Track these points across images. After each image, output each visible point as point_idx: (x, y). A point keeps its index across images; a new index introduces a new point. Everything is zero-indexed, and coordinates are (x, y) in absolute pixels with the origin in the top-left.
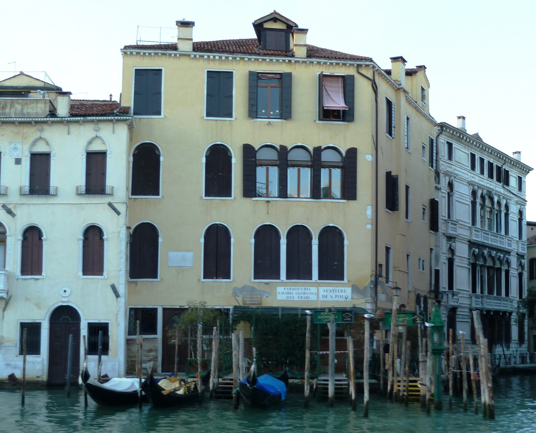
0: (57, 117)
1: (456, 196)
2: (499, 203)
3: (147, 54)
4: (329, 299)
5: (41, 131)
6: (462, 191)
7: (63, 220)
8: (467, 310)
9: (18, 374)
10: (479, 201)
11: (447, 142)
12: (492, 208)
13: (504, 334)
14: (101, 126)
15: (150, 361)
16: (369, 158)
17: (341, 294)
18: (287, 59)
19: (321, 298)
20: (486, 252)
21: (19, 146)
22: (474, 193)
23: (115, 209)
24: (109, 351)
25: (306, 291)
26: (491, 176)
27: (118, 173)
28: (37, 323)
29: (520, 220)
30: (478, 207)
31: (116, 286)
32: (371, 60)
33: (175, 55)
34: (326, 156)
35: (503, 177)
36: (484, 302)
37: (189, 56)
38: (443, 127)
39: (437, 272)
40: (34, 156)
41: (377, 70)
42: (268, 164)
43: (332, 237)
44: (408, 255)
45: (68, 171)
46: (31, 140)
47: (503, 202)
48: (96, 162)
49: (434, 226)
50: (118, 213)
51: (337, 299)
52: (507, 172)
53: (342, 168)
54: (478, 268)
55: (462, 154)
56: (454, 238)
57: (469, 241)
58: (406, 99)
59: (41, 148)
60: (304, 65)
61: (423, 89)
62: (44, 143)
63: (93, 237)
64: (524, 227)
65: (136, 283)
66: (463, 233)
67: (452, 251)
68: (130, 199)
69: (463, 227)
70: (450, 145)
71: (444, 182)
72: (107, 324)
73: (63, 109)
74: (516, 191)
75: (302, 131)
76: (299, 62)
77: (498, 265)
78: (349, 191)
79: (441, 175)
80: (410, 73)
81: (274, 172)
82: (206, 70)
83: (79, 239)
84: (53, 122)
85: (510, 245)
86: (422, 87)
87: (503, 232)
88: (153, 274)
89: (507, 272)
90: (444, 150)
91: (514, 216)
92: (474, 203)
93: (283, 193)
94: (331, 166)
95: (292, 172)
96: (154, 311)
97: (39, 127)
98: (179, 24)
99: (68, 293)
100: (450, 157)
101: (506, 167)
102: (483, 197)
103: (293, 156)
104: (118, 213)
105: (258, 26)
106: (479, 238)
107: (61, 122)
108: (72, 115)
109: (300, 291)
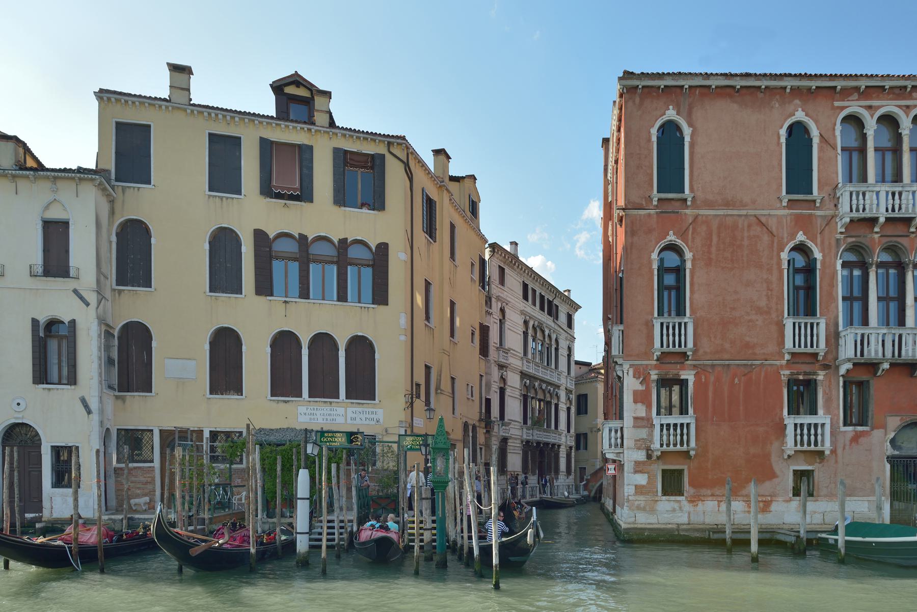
1: (508, 324)
2: (549, 336)
4: (358, 420)
6: (515, 320)
8: (519, 441)
10: (530, 331)
13: (553, 466)
14: (60, 184)
15: (145, 495)
17: (372, 416)
18: (306, 127)
19: (349, 421)
20: (537, 384)
22: (526, 323)
23: (81, 298)
29: (569, 356)
30: (530, 339)
31: (87, 399)
32: (403, 138)
34: (354, 253)
35: (552, 311)
37: (185, 110)
38: (494, 247)
39: (488, 401)
41: (412, 153)
43: (361, 348)
44: (453, 379)
47: (554, 337)
49: (484, 350)
50: (87, 304)
51: (367, 422)
52: (557, 307)
53: (373, 266)
54: (529, 400)
55: (514, 281)
56: (507, 367)
65: (123, 399)
66: (515, 362)
67: (503, 380)
68: (115, 290)
70: (502, 270)
75: (323, 218)
76: (320, 131)
78: (380, 296)
79: (493, 300)
81: (294, 267)
82: (207, 132)
85: (559, 379)
87: (553, 366)
88: (147, 387)
89: (557, 406)
91: (563, 352)
92: (525, 334)
95: (314, 269)
100: (502, 281)
101: (556, 302)
103: (315, 250)
104: (87, 304)
105: (278, 88)
106: (531, 370)
109: (326, 412)
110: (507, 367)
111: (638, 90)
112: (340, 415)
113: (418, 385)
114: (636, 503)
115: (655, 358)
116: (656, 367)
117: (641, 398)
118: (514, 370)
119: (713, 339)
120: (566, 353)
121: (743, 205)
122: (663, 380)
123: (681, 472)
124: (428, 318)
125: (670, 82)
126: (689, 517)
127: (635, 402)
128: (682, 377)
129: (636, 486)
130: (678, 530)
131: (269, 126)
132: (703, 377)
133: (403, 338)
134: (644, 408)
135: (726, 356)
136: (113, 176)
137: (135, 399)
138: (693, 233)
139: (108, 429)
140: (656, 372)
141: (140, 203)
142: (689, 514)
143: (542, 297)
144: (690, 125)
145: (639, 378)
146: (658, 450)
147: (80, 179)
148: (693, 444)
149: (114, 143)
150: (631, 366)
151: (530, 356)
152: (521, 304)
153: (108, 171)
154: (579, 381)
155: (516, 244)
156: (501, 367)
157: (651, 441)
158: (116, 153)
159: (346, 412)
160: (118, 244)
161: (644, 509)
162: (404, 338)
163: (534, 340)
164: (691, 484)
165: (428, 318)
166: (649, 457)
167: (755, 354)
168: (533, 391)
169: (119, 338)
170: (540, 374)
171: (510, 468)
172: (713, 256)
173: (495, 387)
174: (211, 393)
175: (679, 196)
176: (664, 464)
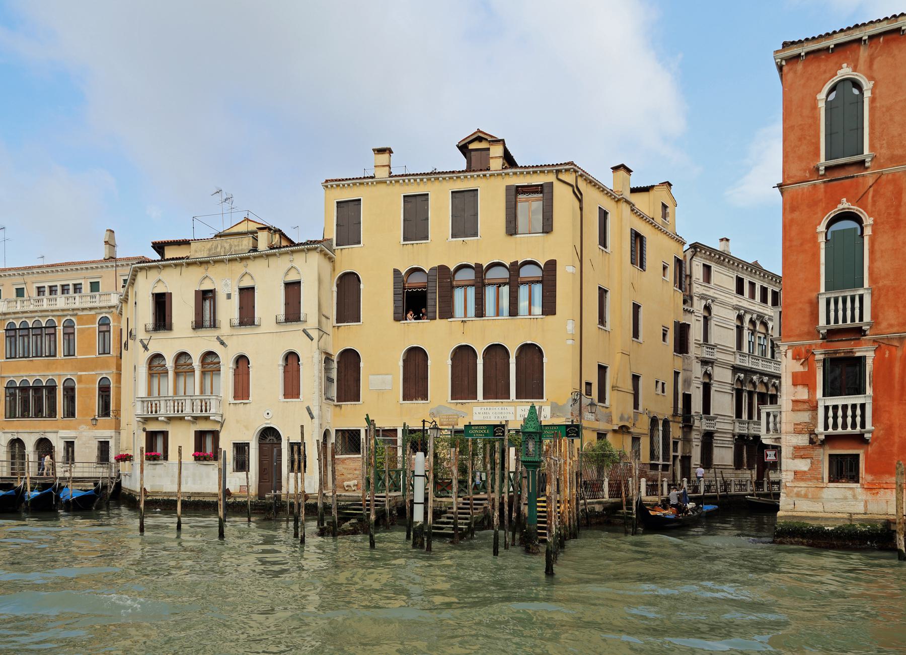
5: (246, 266)
6: (725, 316)
7: (266, 345)
11: (704, 265)
14: (296, 256)
20: (755, 378)
21: (229, 282)
22: (740, 318)
23: (308, 335)
30: (746, 333)
32: (572, 163)
33: (372, 183)
36: (750, 428)
39: (687, 398)
40: (242, 290)
41: (581, 176)
43: (531, 354)
45: (270, 304)
46: (239, 275)
48: (293, 288)
50: (312, 339)
55: (724, 278)
56: (712, 363)
58: (632, 210)
59: (246, 283)
60: (500, 177)
61: (665, 207)
67: (708, 375)
69: (724, 351)
70: (707, 269)
71: (698, 306)
73: (263, 245)
78: (549, 308)
79: (695, 299)
81: (471, 292)
84: (255, 257)
86: (663, 204)
90: (698, 272)
92: (740, 329)
93: (480, 312)
94: (531, 282)
97: (244, 263)
102: (752, 322)
104: (312, 339)
105: (463, 148)
106: (748, 363)
107: (261, 256)
108: (272, 248)
110: (712, 363)
111: (797, 59)
112: (511, 412)
113: (589, 384)
114: (795, 490)
116: (821, 346)
118: (723, 365)
123: (858, 455)
126: (866, 506)
127: (795, 384)
128: (858, 354)
129: (796, 473)
132: (887, 352)
134: (806, 390)
137: (348, 406)
138: (873, 197)
140: (822, 351)
141: (350, 259)
142: (866, 502)
144: (871, 78)
145: (800, 359)
146: (821, 434)
147: (308, 250)
148: (869, 426)
149: (335, 218)
150: (790, 347)
151: (746, 349)
156: (705, 362)
157: (815, 425)
161: (806, 496)
164: (867, 470)
166: (812, 442)
169: (338, 362)
170: (760, 366)
171: (716, 460)
174: (404, 400)
176: (832, 448)
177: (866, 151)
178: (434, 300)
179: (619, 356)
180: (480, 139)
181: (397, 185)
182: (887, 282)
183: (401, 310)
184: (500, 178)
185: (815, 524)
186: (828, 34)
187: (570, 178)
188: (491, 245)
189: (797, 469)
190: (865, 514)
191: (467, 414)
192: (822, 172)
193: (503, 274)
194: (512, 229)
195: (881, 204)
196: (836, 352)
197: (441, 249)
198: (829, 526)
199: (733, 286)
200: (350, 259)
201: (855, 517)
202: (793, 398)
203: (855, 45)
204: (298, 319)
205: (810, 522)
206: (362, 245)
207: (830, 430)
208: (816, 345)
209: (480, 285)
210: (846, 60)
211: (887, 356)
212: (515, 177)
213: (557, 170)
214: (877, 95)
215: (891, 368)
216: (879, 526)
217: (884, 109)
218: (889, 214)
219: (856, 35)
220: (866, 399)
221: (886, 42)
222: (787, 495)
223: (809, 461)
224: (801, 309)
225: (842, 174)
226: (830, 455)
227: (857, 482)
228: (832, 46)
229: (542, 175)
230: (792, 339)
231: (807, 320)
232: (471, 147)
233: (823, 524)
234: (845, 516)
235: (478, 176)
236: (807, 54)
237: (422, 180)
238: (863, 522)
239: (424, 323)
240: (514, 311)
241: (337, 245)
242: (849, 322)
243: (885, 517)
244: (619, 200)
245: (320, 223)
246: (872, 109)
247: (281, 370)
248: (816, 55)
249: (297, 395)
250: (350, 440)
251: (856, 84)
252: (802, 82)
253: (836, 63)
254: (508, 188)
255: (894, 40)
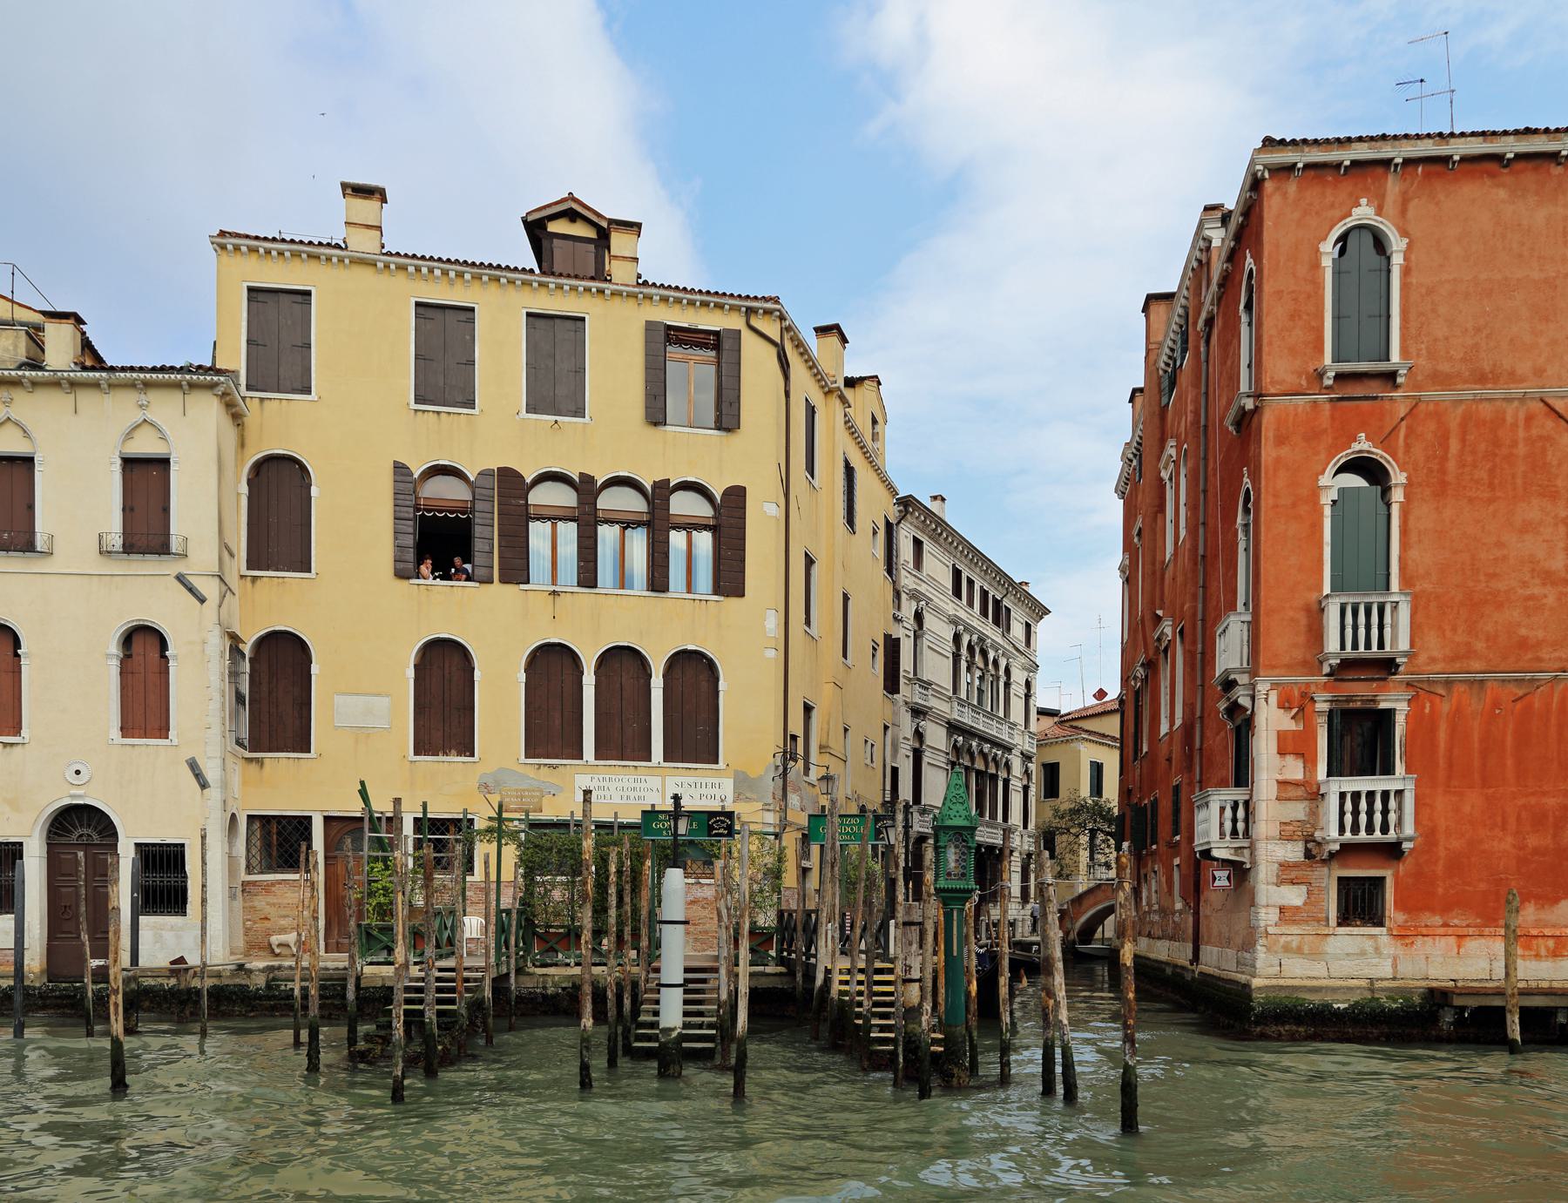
0: (41, 369)
2: (995, 662)
3: (274, 253)
5: (8, 403)
9: (193, 960)
12: (984, 671)
14: (154, 396)
16: (774, 511)
22: (957, 638)
23: (191, 590)
24: (188, 906)
25: (637, 785)
26: (984, 613)
27: (205, 507)
28: (14, 844)
29: (1028, 696)
30: (964, 665)
33: (341, 260)
34: (684, 505)
35: (1000, 617)
39: (895, 771)
42: (554, 517)
43: (694, 672)
44: (846, 730)
47: (1003, 663)
48: (146, 477)
50: (202, 600)
52: (1008, 610)
55: (938, 566)
56: (925, 714)
57: (948, 723)
62: (19, 433)
63: (143, 648)
64: (1033, 715)
67: (919, 735)
70: (918, 543)
72: (183, 845)
74: (1022, 646)
77: (992, 770)
78: (729, 578)
79: (904, 596)
80: (851, 383)
81: (568, 531)
83: (108, 656)
84: (35, 384)
87: (1001, 714)
89: (1006, 782)
91: (1018, 689)
92: (956, 657)
94: (690, 526)
96: (304, 823)
98: (349, 191)
99: (84, 777)
102: (971, 648)
104: (202, 600)
105: (536, 228)
106: (967, 718)
107: (56, 384)
110: (925, 714)
115: (1326, 669)
116: (1325, 687)
117: (1291, 745)
119: (1448, 634)
120: (1022, 691)
121: (1514, 378)
122: (1346, 713)
123: (1383, 878)
124: (808, 622)
125: (1363, 152)
126: (1395, 966)
128: (1383, 705)
129: (1282, 909)
130: (1372, 990)
131: (527, 288)
133: (771, 653)
134: (1300, 764)
135: (1477, 665)
136: (243, 380)
137: (279, 763)
138: (1406, 437)
139: (233, 815)
140: (1328, 696)
141: (282, 425)
142: (1395, 959)
143: (984, 594)
144: (1404, 233)
146: (1335, 841)
147: (192, 386)
149: (244, 324)
150: (1274, 686)
152: (950, 607)
153: (235, 373)
154: (1043, 742)
155: (943, 500)
156: (918, 712)
158: (249, 342)
159: (664, 785)
160: (250, 498)
161: (1299, 951)
162: (773, 655)
163: (968, 669)
165: (808, 622)
166: (1308, 855)
167: (1539, 660)
168: (967, 757)
172: (1450, 478)
173: (906, 750)
174: (416, 753)
175: (1382, 366)
176: (1344, 866)
177: (1395, 357)
178: (488, 538)
179: (828, 689)
180: (572, 216)
181: (401, 276)
182: (1427, 586)
183: (410, 555)
184: (631, 302)
185: (1316, 999)
186: (1338, 140)
187: (772, 329)
188: (610, 436)
189: (1285, 902)
190: (1394, 979)
191: (561, 790)
192: (1328, 382)
193: (563, 497)
194: (656, 416)
195: (1418, 451)
196: (1349, 699)
197: (497, 431)
198: (1338, 1002)
199: (948, 583)
200: (282, 425)
201: (1378, 985)
202: (1280, 778)
203: (1380, 170)
204: (160, 546)
205: (1308, 996)
206: (314, 396)
207: (1348, 834)
208: (1316, 684)
209: (588, 520)
210: (1366, 191)
211: (1427, 710)
212: (662, 306)
213: (750, 308)
214: (1413, 264)
215: (1433, 730)
216: (1417, 1000)
217: (1423, 291)
218: (1431, 470)
219: (1386, 151)
220: (1400, 780)
221: (1426, 175)
222: (1268, 949)
223: (1304, 888)
224: (1292, 620)
225: (1358, 390)
226: (1340, 879)
227: (1381, 924)
228: (1347, 163)
229: (718, 312)
230: (1277, 671)
231: (1301, 639)
232: (553, 227)
233: (1328, 998)
234: (1364, 983)
235: (588, 290)
236: (1307, 166)
237: (460, 275)
238: (1393, 993)
239: (460, 590)
240: (658, 581)
241: (249, 388)
242: (1375, 648)
243: (1424, 984)
244: (830, 392)
245: (216, 332)
246: (1405, 287)
247: (114, 667)
248: (1319, 172)
249: (161, 729)
250: (280, 841)
251: (1380, 244)
252: (1296, 215)
253: (1351, 194)
254: (650, 327)
255: (1439, 175)
